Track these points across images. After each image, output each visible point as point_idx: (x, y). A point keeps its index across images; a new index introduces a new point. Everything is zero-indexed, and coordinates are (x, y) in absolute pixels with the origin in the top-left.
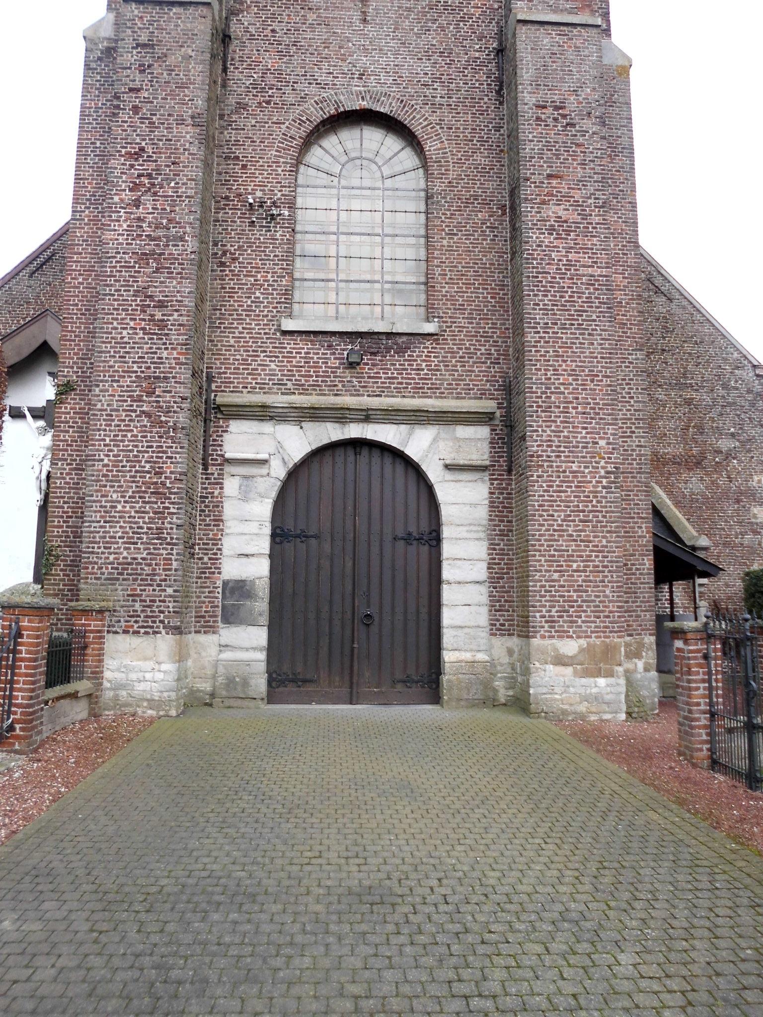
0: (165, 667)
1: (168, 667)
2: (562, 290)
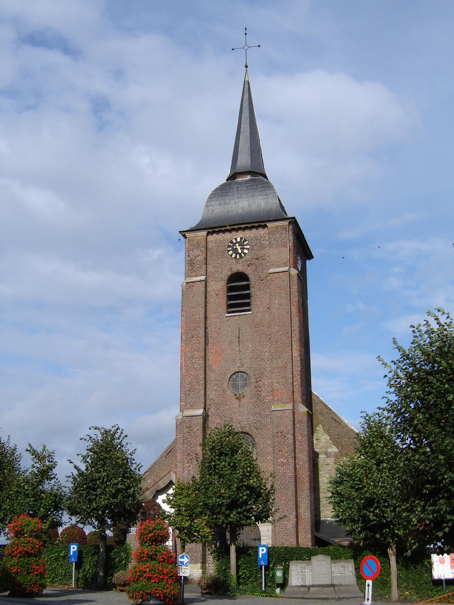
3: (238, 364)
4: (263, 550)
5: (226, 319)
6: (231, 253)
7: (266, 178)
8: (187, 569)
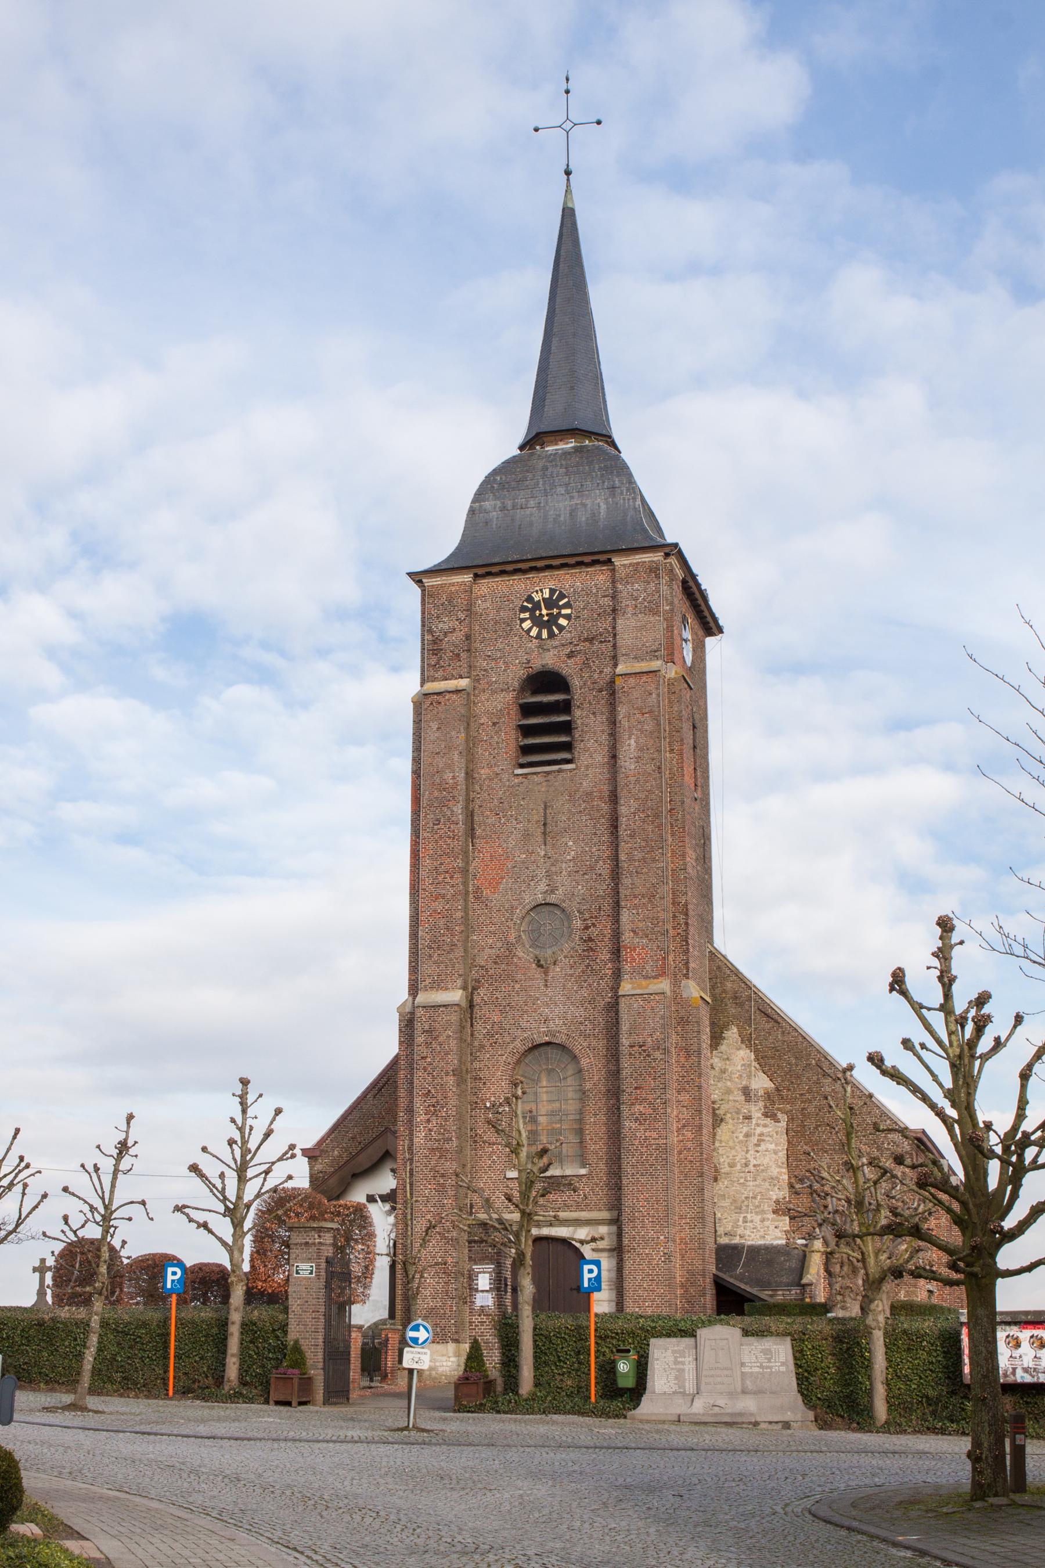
2: (642, 1154)
3: (543, 887)
6: (527, 625)
7: (613, 445)
8: (425, 1353)
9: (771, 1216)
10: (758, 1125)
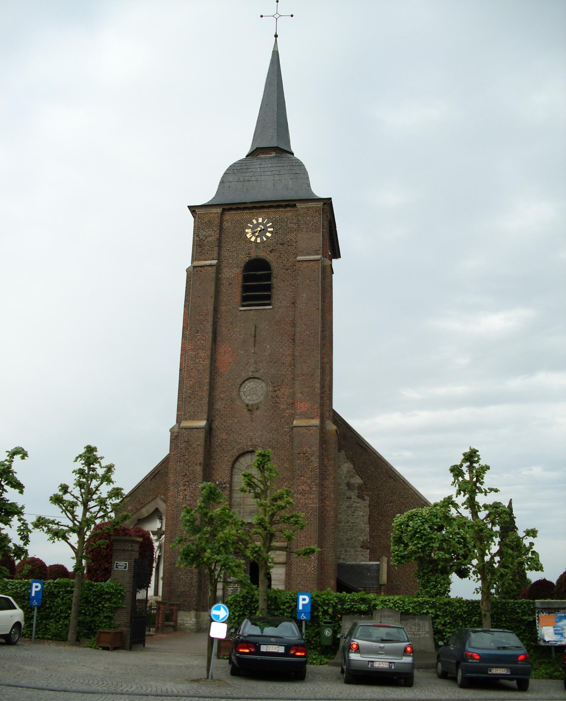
0: (193, 620)
1: (194, 620)
4: (304, 600)
5: (239, 314)
9: (359, 549)
10: (354, 502)
